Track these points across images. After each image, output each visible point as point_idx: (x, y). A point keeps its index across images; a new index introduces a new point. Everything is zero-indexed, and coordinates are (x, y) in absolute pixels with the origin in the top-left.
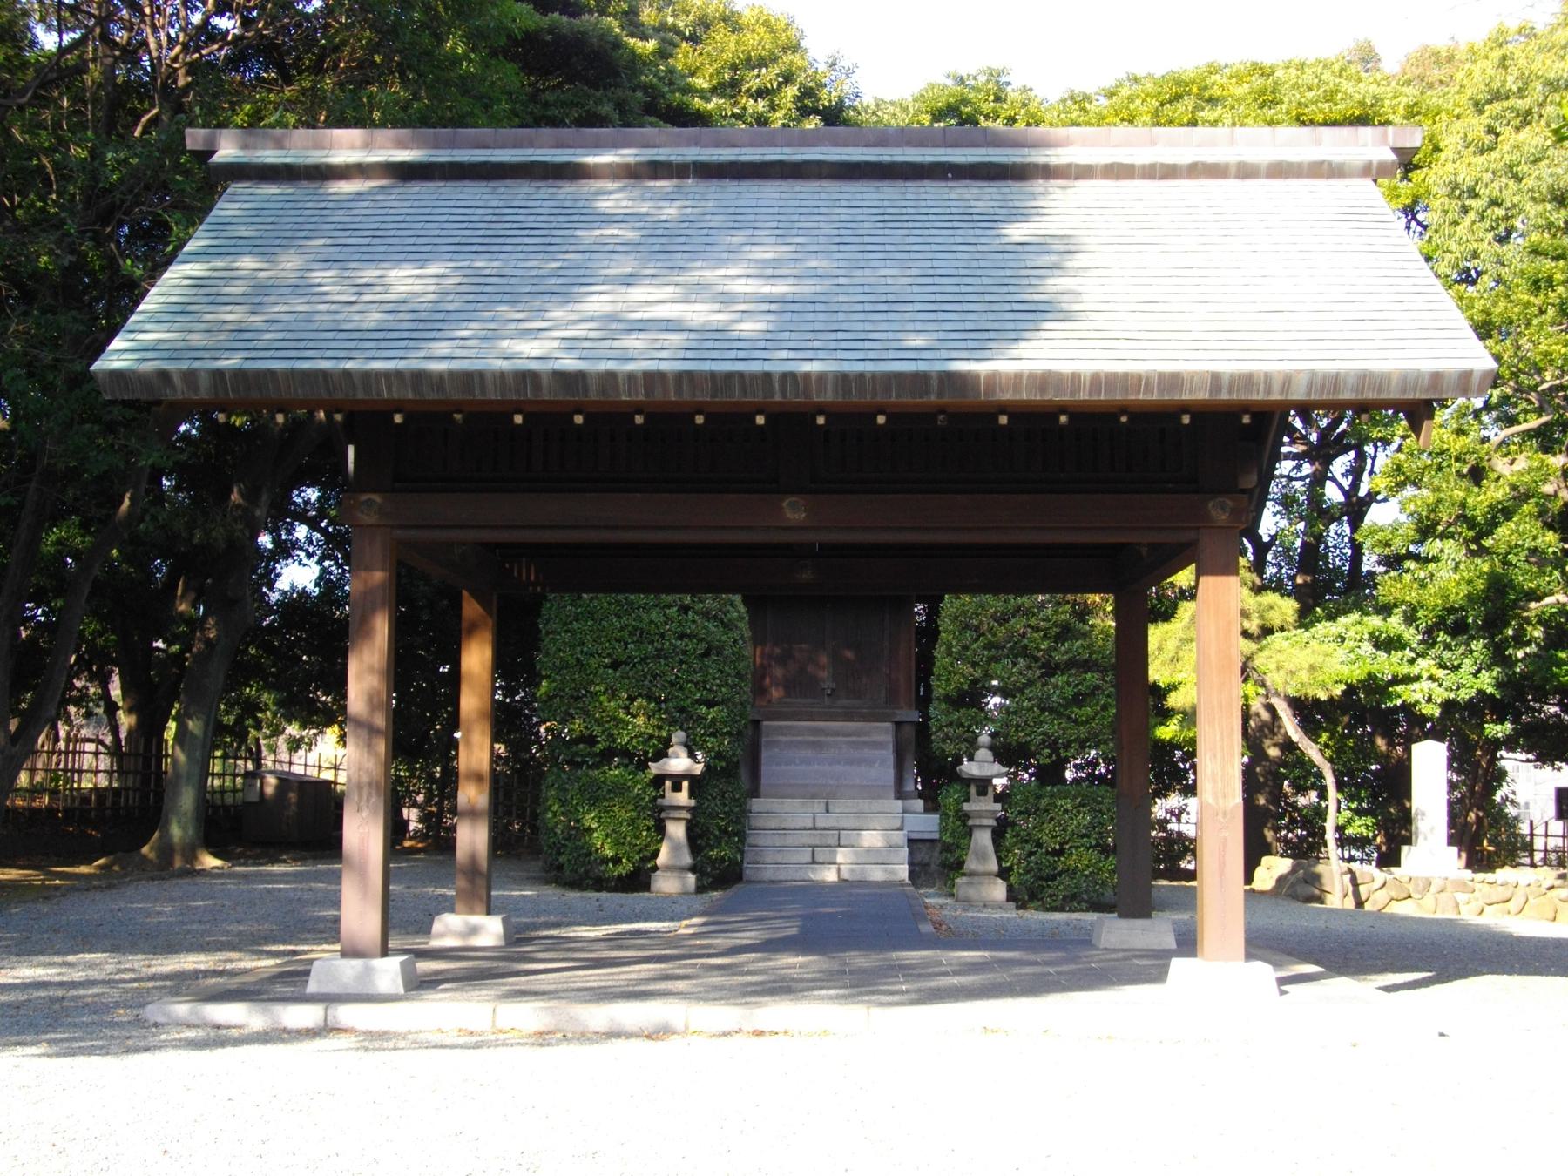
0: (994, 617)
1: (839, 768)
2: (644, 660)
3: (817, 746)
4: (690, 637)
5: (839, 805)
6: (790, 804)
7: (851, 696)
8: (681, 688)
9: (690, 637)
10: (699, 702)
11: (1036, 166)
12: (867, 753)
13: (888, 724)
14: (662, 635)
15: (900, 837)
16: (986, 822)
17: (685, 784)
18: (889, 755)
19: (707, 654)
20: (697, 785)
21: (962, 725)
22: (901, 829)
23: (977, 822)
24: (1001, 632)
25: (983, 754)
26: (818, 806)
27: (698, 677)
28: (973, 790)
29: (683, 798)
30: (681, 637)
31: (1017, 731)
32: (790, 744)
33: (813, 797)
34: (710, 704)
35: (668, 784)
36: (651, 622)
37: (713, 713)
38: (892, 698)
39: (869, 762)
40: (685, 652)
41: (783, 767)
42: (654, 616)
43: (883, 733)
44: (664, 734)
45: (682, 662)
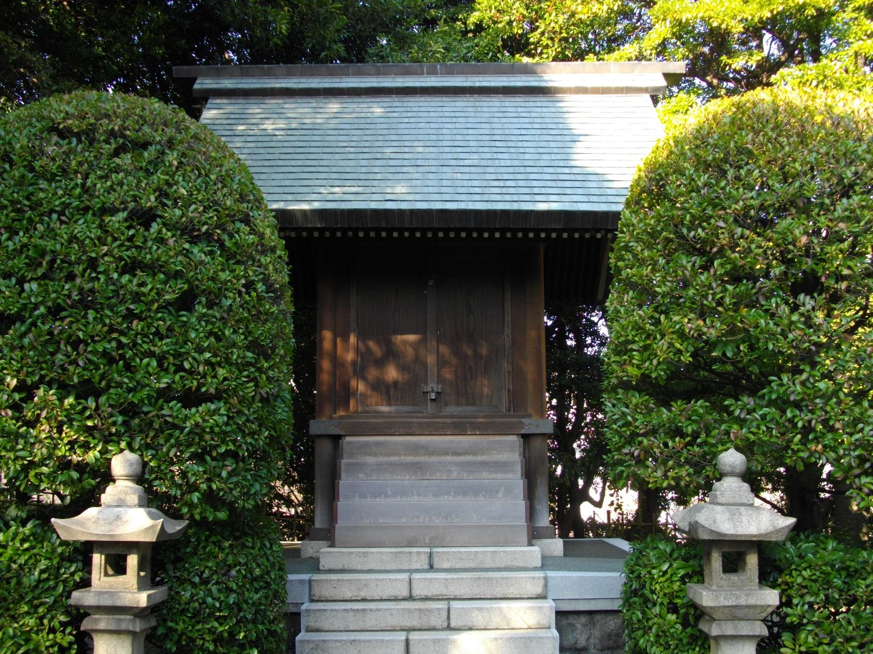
0: (741, 219)
1: (447, 501)
2: (55, 312)
3: (416, 468)
4: (152, 268)
5: (446, 556)
6: (378, 556)
7: (456, 404)
8: (128, 367)
9: (152, 268)
10: (165, 395)
11: (555, 88)
12: (487, 478)
13: (514, 438)
14: (93, 264)
15: (546, 611)
16: (745, 629)
17: (132, 561)
18: (519, 484)
19: (186, 302)
20: (158, 559)
21: (678, 432)
22: (542, 597)
23: (729, 629)
24: (760, 245)
25: (732, 487)
26: (417, 556)
27: (163, 346)
28: (716, 561)
29: (130, 589)
30: (131, 267)
31: (804, 442)
32: (379, 468)
33: (410, 545)
34: (191, 399)
35: (98, 559)
36: (73, 238)
37: (195, 415)
38: (517, 403)
39: (490, 492)
40: (137, 297)
41: (369, 500)
42: (79, 228)
43: (507, 450)
44: (92, 456)
45: (130, 316)
